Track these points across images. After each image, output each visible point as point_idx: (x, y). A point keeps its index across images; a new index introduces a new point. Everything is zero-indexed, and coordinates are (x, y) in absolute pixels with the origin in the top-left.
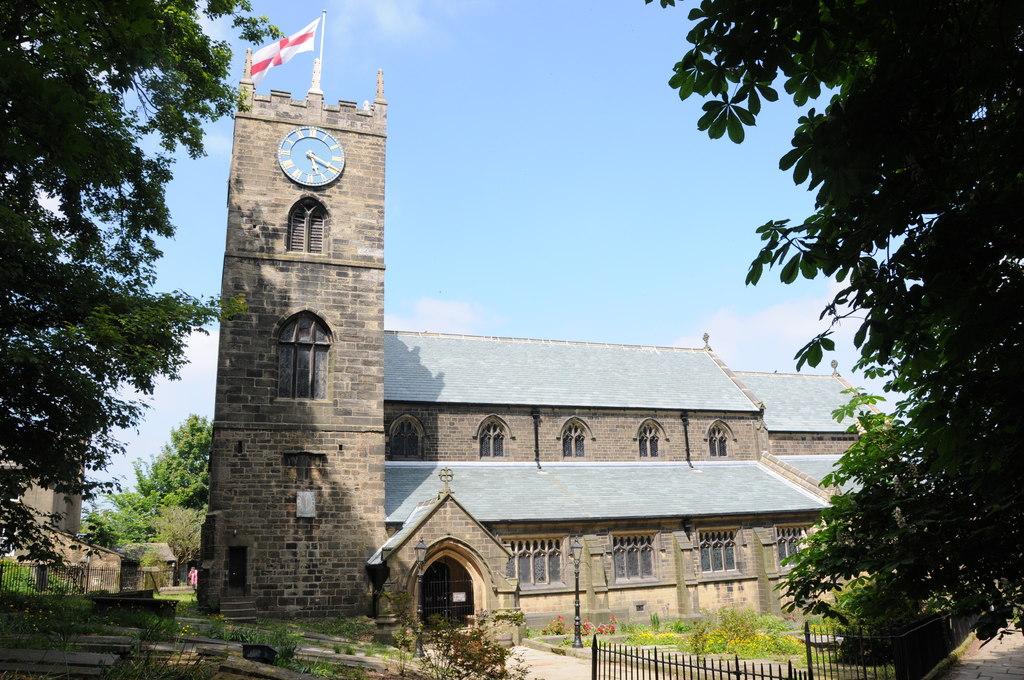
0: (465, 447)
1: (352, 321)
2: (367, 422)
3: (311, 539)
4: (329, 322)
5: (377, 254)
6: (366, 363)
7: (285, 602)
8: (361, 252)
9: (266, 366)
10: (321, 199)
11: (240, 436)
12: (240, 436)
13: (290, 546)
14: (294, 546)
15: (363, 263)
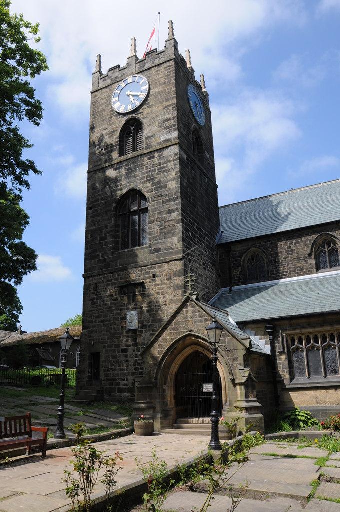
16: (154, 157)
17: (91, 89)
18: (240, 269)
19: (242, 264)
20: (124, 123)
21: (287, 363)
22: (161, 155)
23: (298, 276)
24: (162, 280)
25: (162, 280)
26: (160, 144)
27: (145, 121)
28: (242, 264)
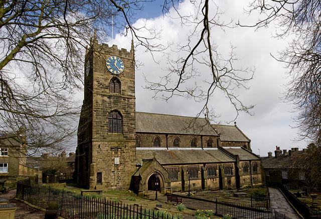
1: (128, 113)
2: (131, 139)
3: (118, 170)
4: (121, 113)
5: (133, 94)
6: (131, 124)
7: (112, 186)
8: (129, 94)
9: (105, 124)
10: (118, 78)
11: (99, 143)
12: (99, 143)
13: (113, 172)
14: (114, 172)
15: (129, 97)
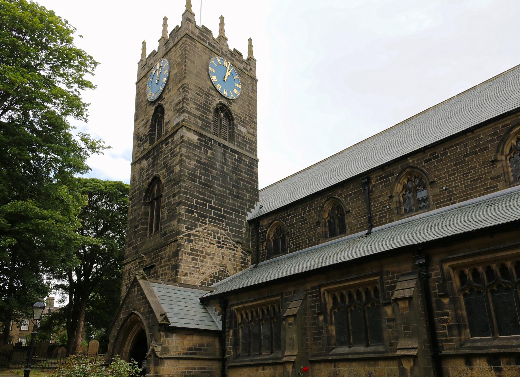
0: (312, 233)
16: (168, 143)
17: (136, 81)
18: (265, 244)
19: (267, 238)
20: (154, 111)
21: (345, 352)
22: (173, 140)
23: (309, 247)
24: (165, 262)
25: (165, 262)
26: (173, 128)
27: (165, 107)
28: (267, 238)
